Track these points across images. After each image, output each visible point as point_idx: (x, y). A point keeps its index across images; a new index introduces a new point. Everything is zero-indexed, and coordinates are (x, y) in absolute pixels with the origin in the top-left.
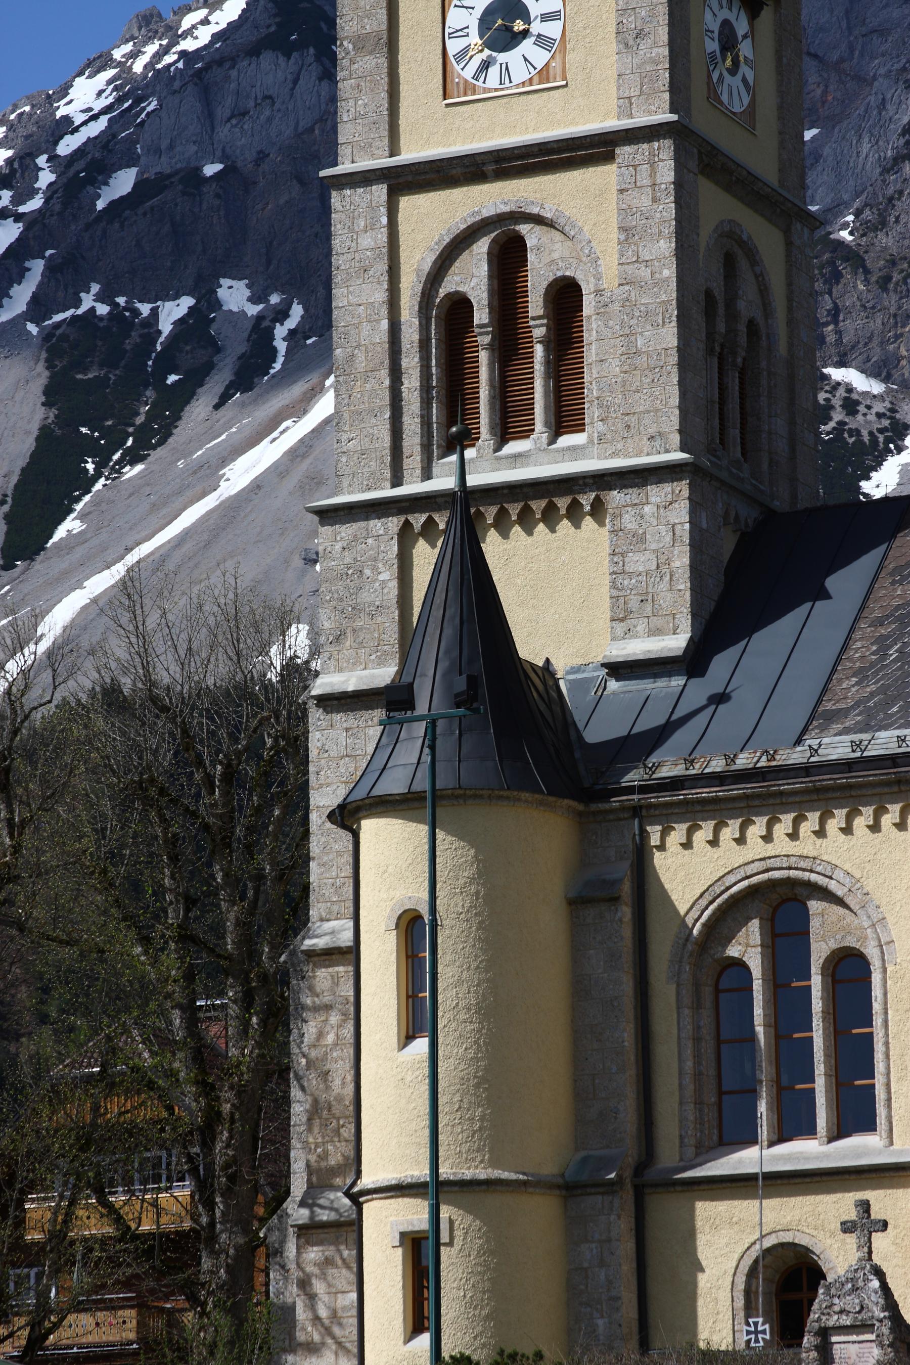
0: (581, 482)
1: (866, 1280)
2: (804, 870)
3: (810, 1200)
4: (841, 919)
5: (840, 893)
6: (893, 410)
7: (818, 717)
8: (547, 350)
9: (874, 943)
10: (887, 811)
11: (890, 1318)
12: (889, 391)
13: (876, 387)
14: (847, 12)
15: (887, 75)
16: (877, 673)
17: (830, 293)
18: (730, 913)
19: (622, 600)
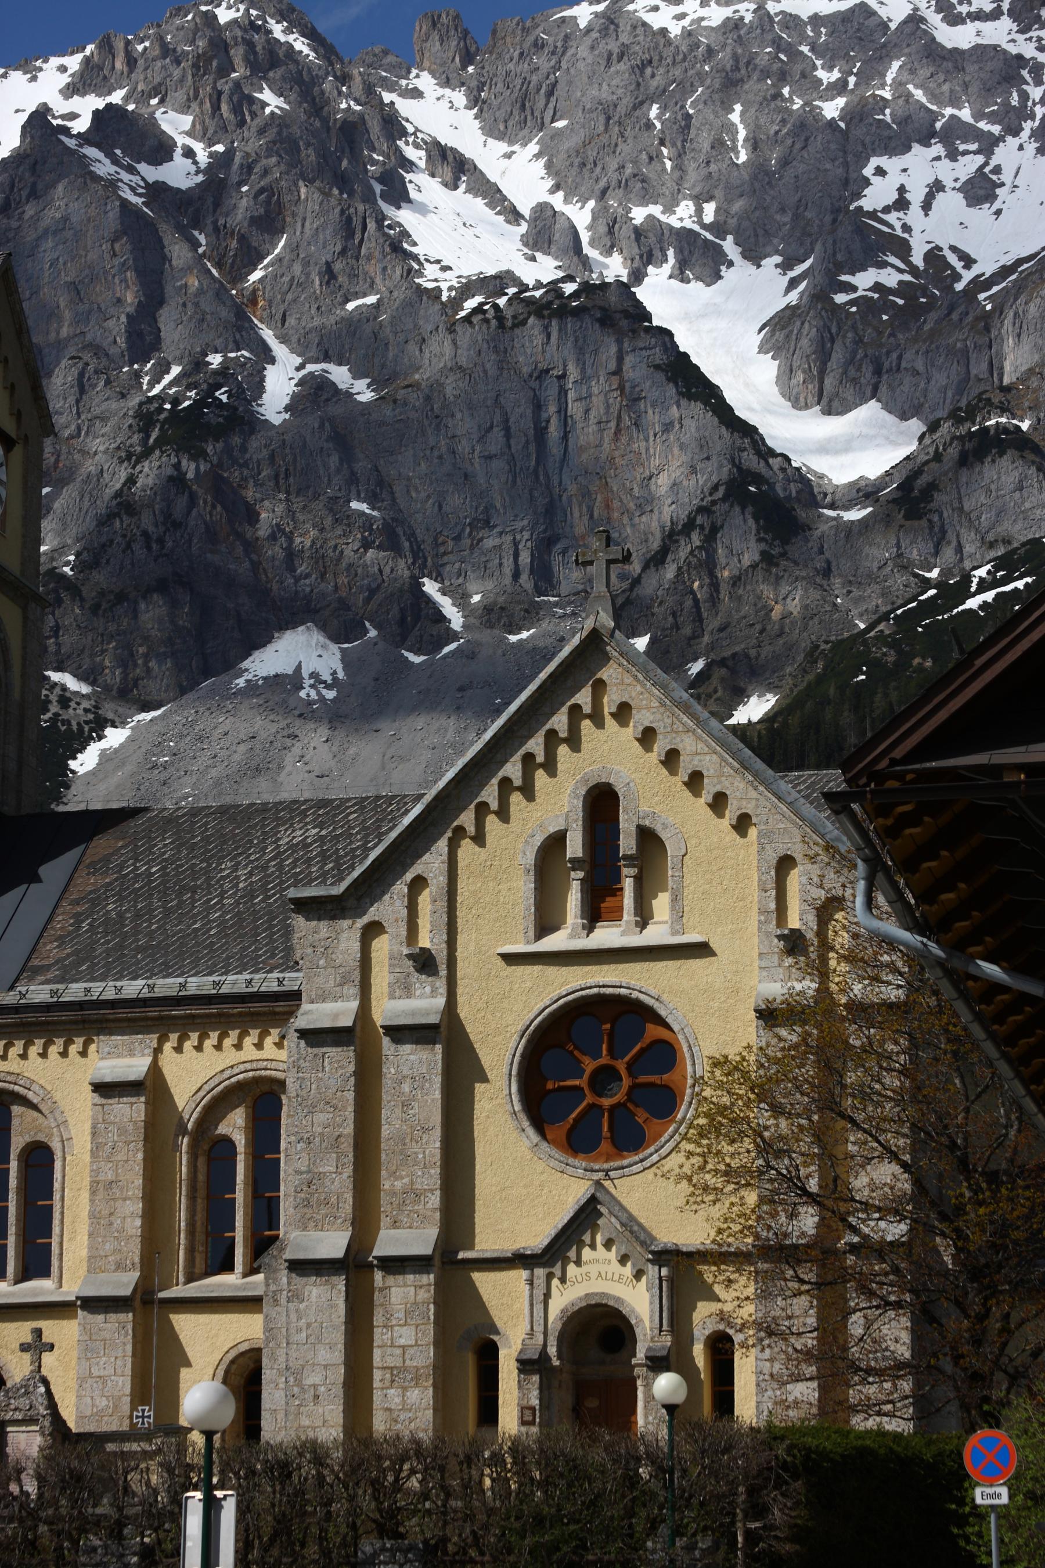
1: (36, 1387)
4: (34, 1120)
5: (35, 1101)
6: (96, 707)
7: (27, 971)
9: (57, 1139)
10: (73, 1042)
12: (94, 692)
13: (85, 689)
14: (78, 401)
15: (106, 452)
16: (72, 940)
17: (53, 614)
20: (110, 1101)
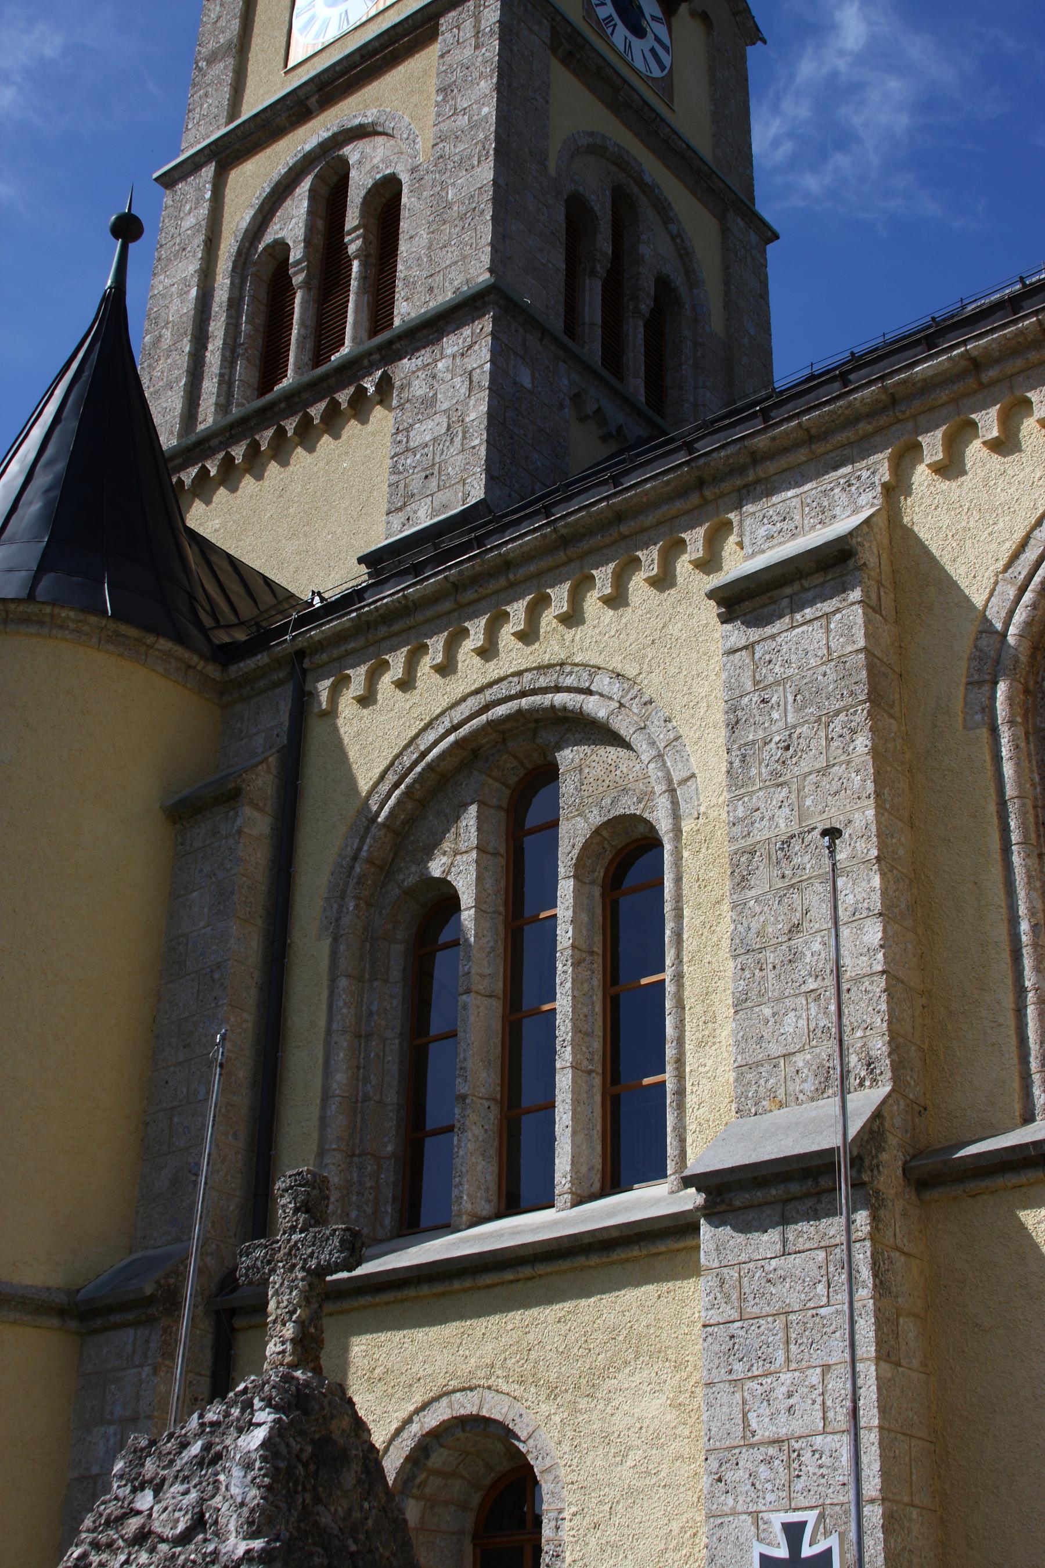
0: (366, 362)
2: (545, 690)
3: (516, 1317)
8: (363, 265)
18: (433, 791)
19: (402, 485)
20: (769, 630)
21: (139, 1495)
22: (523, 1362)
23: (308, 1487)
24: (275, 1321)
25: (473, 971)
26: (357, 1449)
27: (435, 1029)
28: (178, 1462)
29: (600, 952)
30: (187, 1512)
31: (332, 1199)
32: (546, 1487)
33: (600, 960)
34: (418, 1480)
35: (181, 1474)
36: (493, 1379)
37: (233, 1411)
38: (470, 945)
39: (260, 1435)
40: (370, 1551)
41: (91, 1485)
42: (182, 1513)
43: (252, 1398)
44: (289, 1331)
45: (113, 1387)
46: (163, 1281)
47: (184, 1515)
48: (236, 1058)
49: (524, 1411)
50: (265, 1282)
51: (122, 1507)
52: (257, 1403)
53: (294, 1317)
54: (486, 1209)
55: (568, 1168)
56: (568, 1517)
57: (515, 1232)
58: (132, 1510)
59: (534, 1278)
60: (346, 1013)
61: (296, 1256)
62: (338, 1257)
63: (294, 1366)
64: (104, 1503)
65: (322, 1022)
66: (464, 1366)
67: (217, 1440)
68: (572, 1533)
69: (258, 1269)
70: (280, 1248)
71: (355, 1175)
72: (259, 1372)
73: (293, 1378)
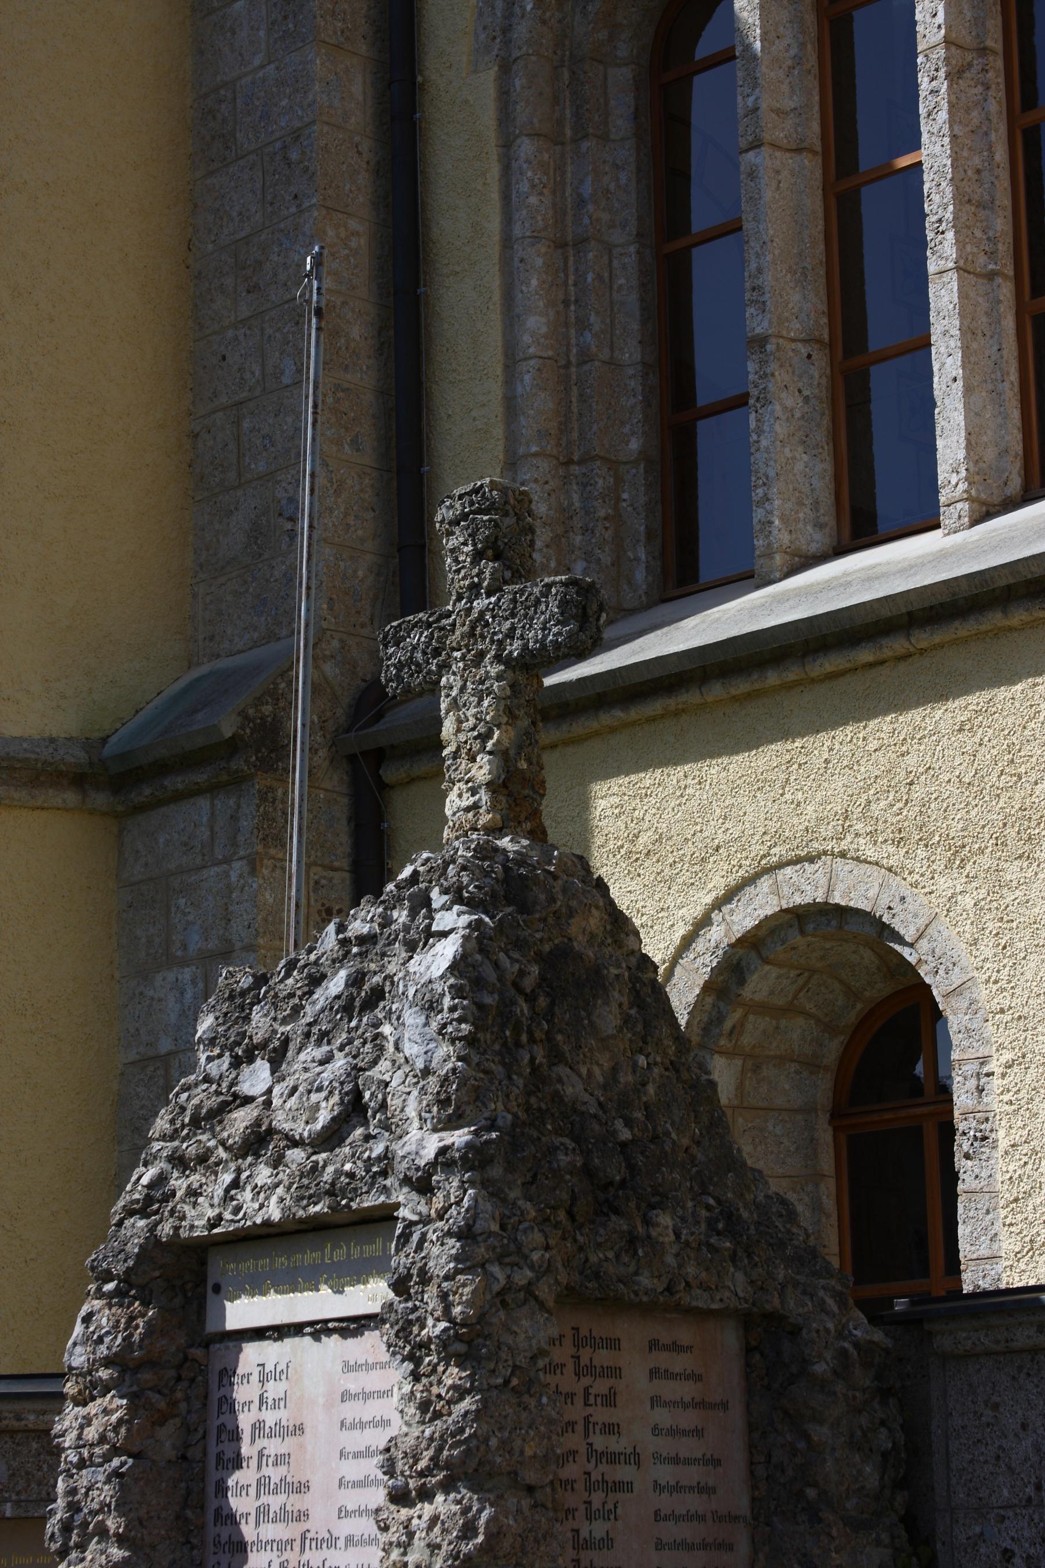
11: (472, 1160)
21: (246, 1070)
22: (900, 805)
23: (539, 1035)
24: (456, 755)
25: (764, 106)
26: (619, 966)
27: (701, 220)
28: (308, 1009)
29: (999, 47)
30: (331, 1092)
31: (539, 544)
32: (956, 1020)
33: (1000, 63)
34: (728, 1024)
35: (315, 1030)
36: (849, 838)
37: (395, 914)
38: (755, 57)
39: (446, 951)
40: (655, 1138)
41: (159, 1068)
42: (324, 1094)
43: (428, 890)
44: (482, 770)
45: (182, 901)
46: (251, 712)
47: (326, 1099)
48: (344, 303)
49: (907, 892)
50: (433, 688)
51: (218, 1093)
52: (437, 898)
53: (489, 745)
54: (817, 540)
55: (961, 454)
56: (998, 1071)
57: (871, 577)
58: (235, 1096)
59: (910, 655)
60: (535, 203)
61: (483, 638)
62: (559, 634)
63: (495, 830)
64: (186, 1088)
65: (494, 224)
66: (796, 820)
67: (373, 966)
68: (1006, 1097)
69: (418, 665)
70: (454, 625)
71: (576, 497)
72: (437, 845)
73: (496, 850)
